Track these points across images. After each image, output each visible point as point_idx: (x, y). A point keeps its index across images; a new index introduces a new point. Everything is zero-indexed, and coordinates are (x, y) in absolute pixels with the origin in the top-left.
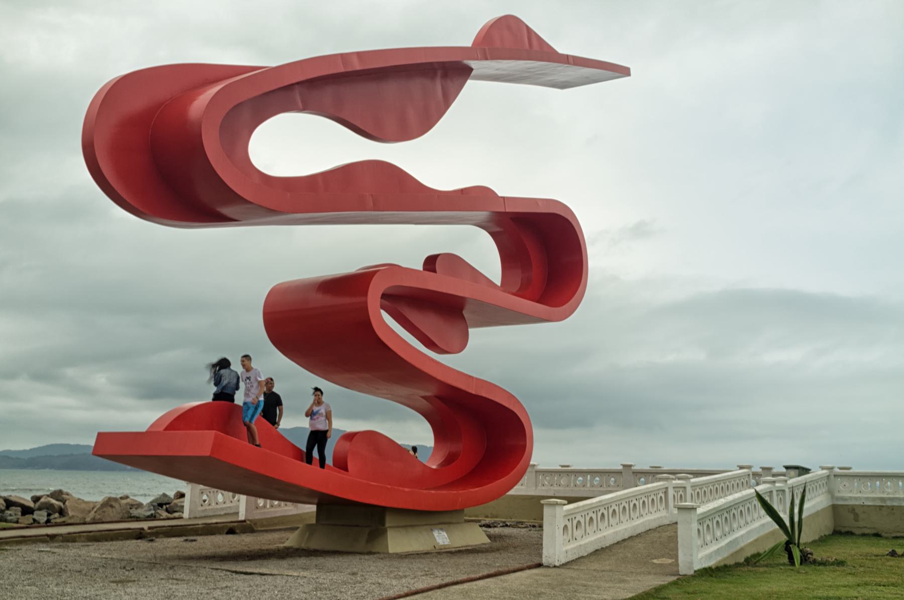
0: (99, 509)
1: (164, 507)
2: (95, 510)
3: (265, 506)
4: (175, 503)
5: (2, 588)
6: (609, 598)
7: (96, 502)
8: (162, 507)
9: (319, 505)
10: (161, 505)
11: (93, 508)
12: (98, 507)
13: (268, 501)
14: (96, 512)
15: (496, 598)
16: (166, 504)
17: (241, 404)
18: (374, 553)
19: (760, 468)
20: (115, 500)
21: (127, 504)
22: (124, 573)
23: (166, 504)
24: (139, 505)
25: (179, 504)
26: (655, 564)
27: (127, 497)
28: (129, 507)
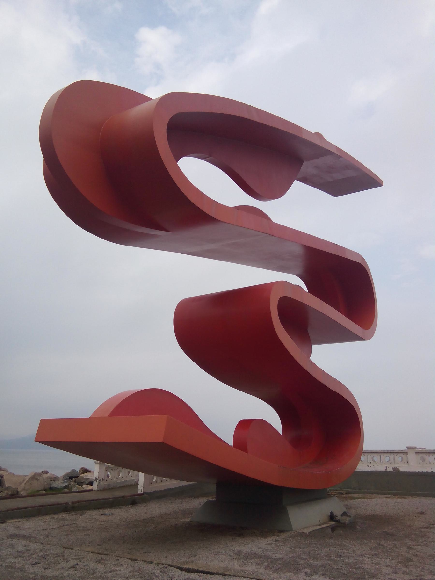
0: (28, 481)
1: (74, 479)
2: (25, 482)
3: (156, 482)
4: (82, 477)
5: (171, 579)
6: (413, 579)
7: (25, 476)
8: (72, 479)
9: (219, 485)
10: (71, 478)
11: (23, 481)
12: (27, 480)
13: (159, 478)
14: (25, 484)
15: (82, 578)
16: (75, 477)
17: (392, 470)
18: (287, 531)
19: (407, 447)
20: (39, 475)
21: (48, 478)
22: (29, 554)
23: (75, 477)
24: (55, 479)
25: (85, 477)
26: (326, 524)
27: (47, 472)
28: (49, 480)
